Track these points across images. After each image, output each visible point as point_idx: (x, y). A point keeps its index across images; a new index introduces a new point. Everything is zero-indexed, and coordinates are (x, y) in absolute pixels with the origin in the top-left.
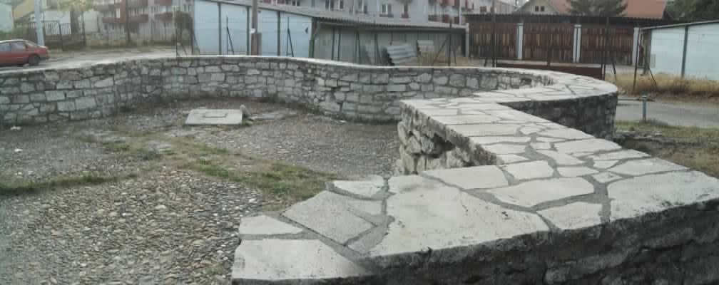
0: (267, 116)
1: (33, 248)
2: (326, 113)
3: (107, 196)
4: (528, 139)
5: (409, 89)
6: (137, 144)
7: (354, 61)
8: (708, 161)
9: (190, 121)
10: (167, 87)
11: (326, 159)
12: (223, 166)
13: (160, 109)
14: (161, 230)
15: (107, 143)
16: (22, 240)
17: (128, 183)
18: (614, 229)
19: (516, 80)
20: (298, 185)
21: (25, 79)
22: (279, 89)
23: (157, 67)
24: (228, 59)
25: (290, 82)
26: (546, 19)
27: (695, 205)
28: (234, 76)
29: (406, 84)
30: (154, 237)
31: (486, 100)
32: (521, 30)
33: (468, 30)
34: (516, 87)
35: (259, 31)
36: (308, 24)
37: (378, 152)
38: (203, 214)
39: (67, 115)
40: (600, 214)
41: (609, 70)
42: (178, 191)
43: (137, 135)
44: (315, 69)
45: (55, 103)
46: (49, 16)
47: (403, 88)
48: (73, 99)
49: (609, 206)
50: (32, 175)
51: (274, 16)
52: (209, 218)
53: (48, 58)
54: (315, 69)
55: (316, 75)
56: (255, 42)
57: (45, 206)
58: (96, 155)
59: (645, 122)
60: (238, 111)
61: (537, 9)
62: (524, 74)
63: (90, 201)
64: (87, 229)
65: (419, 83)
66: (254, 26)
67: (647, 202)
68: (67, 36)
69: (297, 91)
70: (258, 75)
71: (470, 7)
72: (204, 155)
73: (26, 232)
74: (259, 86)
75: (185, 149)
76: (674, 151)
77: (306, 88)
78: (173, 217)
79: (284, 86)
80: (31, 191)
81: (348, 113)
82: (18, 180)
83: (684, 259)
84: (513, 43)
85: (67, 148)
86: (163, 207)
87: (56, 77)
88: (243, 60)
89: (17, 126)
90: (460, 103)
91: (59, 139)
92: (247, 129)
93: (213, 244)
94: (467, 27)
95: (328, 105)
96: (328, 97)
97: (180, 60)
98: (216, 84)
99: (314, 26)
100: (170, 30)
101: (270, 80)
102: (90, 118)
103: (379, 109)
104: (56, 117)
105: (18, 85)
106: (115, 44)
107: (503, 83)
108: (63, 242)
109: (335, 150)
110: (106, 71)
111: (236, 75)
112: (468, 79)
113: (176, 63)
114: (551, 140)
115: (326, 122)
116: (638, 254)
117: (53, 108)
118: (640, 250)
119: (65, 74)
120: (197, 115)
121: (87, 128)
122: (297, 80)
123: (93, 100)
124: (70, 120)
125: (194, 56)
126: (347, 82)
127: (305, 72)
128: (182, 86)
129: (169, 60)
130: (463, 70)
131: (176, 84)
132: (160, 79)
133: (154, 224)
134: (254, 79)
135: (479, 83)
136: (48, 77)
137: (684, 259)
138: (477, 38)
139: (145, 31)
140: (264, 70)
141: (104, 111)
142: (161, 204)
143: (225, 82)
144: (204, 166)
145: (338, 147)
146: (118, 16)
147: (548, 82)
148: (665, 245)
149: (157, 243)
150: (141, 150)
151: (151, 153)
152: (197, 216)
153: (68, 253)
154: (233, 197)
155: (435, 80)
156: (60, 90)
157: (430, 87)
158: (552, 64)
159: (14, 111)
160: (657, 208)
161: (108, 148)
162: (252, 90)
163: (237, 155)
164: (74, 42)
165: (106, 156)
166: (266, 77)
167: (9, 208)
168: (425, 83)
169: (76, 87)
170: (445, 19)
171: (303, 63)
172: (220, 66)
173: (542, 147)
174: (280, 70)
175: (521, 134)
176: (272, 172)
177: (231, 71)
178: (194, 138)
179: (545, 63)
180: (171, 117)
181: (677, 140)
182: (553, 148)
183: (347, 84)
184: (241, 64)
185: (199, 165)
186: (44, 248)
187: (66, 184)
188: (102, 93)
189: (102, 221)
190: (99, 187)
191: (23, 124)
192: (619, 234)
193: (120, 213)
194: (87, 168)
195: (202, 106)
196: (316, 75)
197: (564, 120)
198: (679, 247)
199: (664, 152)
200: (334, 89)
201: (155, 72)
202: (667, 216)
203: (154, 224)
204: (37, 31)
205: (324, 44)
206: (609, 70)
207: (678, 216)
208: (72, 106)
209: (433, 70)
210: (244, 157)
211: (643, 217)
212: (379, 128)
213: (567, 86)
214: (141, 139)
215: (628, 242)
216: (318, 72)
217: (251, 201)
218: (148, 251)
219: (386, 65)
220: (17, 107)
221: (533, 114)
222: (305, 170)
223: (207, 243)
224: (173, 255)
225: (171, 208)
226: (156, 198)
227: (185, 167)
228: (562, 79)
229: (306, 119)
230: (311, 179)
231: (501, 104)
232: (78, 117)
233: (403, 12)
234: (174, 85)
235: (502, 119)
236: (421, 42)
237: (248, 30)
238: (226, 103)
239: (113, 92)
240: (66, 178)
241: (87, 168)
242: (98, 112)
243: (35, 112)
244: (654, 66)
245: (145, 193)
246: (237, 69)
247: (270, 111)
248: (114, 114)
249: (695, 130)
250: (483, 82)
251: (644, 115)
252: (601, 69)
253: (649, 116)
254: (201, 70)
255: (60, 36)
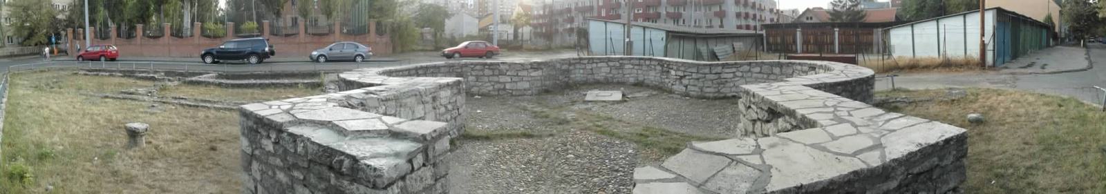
0: (638, 95)
1: (489, 175)
2: (677, 92)
3: (535, 146)
4: (832, 109)
5: (735, 76)
6: (553, 114)
7: (693, 59)
8: (938, 110)
9: (588, 98)
10: (572, 76)
11: (678, 123)
12: (611, 129)
13: (568, 90)
14: (571, 171)
15: (535, 112)
16: (481, 169)
17: (549, 139)
18: (890, 166)
19: (805, 68)
20: (660, 141)
21: (487, 67)
22: (646, 77)
23: (566, 64)
24: (612, 58)
25: (652, 73)
26: (814, 25)
27: (937, 143)
28: (616, 69)
29: (734, 73)
30: (567, 176)
31: (795, 83)
32: (799, 34)
33: (765, 35)
34: (806, 73)
35: (631, 40)
36: (663, 35)
37: (720, 118)
38: (599, 160)
39: (511, 91)
40: (879, 158)
41: (860, 58)
42: (581, 145)
43: (554, 108)
44: (669, 65)
45: (504, 83)
46: (501, 28)
47: (731, 75)
48: (516, 82)
49: (885, 152)
50: (488, 128)
51: (640, 31)
52: (603, 163)
53: (498, 54)
54: (669, 65)
55: (670, 68)
56: (629, 47)
57: (496, 149)
58: (529, 119)
59: (894, 90)
60: (619, 92)
61: (807, 19)
62: (810, 64)
63: (525, 149)
64: (523, 166)
65: (742, 72)
66: (628, 37)
67: (908, 145)
68: (511, 41)
69: (658, 78)
70: (632, 69)
71: (763, 18)
72: (598, 121)
73: (484, 164)
74: (632, 75)
75: (585, 117)
76: (916, 107)
77: (663, 77)
78: (579, 163)
79: (648, 75)
80: (487, 138)
81: (691, 93)
82: (479, 131)
83: (934, 177)
84: (795, 42)
85: (510, 113)
86: (572, 156)
87: (507, 67)
88: (621, 59)
89: (479, 95)
90: (779, 87)
91: (505, 106)
92: (625, 104)
93: (606, 180)
94: (764, 32)
95: (678, 88)
96: (677, 82)
97: (581, 59)
98: (604, 74)
99: (667, 36)
100: (574, 38)
101: (640, 72)
102: (525, 95)
103: (716, 90)
104: (504, 92)
105: (483, 70)
106: (540, 48)
107: (796, 70)
108: (508, 173)
109: (684, 117)
110: (536, 66)
111: (617, 68)
112: (774, 68)
113: (578, 61)
114: (847, 109)
115: (677, 98)
116: (905, 179)
117: (502, 87)
118: (907, 176)
119: (513, 66)
120: (592, 95)
121: (524, 100)
122: (657, 71)
123: (528, 83)
124: (512, 95)
125: (590, 57)
126: (703, 74)
127: (662, 66)
128: (582, 76)
129: (574, 59)
130: (770, 62)
131: (578, 75)
132: (568, 71)
133: (566, 168)
134: (628, 71)
135: (781, 71)
136: (502, 66)
137: (934, 177)
138: (771, 40)
139: (557, 41)
140: (636, 65)
141: (534, 92)
142: (571, 154)
143: (610, 73)
144: (599, 129)
145: (685, 115)
146: (544, 31)
147: (827, 69)
148: (922, 171)
149: (568, 180)
150: (556, 118)
151: (563, 120)
152: (594, 162)
153: (511, 181)
154: (618, 149)
155: (752, 70)
156: (509, 75)
157: (749, 74)
158: (823, 55)
159: (478, 87)
160: (914, 149)
161: (535, 115)
162: (628, 78)
163: (620, 121)
164: (514, 46)
165: (534, 120)
166: (637, 70)
167: (473, 147)
168: (745, 72)
169: (519, 74)
170: (748, 27)
171: (662, 60)
172: (606, 62)
173: (843, 114)
174: (646, 65)
175: (826, 106)
176: (643, 132)
177: (614, 66)
178: (591, 109)
179: (818, 55)
180: (575, 96)
181: (917, 99)
182: (850, 115)
183: (703, 76)
184: (621, 62)
185: (594, 128)
186: (496, 176)
187: (510, 136)
188: (535, 80)
189: (533, 162)
190: (531, 139)
191: (483, 95)
192: (893, 168)
193: (545, 158)
194: (523, 127)
195: (595, 88)
196: (670, 68)
197: (844, 94)
198: (931, 171)
199: (910, 108)
200: (682, 77)
201: (565, 67)
202: (921, 152)
203: (566, 168)
204: (494, 37)
205: (674, 47)
206: (860, 58)
207: (928, 152)
208: (514, 86)
209: (750, 63)
210: (624, 122)
211: (906, 156)
212: (717, 102)
213: (841, 72)
214: (556, 111)
215: (899, 173)
216: (671, 66)
217: (630, 151)
218: (563, 186)
219: (715, 61)
220: (480, 84)
221: (825, 91)
222: (664, 130)
223: (602, 180)
224: (579, 188)
225: (577, 157)
226: (568, 150)
227: (586, 129)
228: (838, 66)
229: (664, 97)
230: (669, 137)
231: (804, 85)
232: (518, 94)
233: (720, 23)
234: (577, 75)
235: (811, 96)
236: (735, 44)
237: (624, 40)
238: (611, 87)
239: (541, 80)
240: (510, 132)
241: (523, 127)
242: (530, 92)
243: (491, 88)
244: (894, 52)
245: (560, 147)
246: (618, 64)
247: (640, 92)
248: (539, 94)
249: (927, 91)
250: (783, 70)
251: (893, 86)
252: (855, 58)
253: (896, 86)
254: (595, 65)
255: (507, 41)
